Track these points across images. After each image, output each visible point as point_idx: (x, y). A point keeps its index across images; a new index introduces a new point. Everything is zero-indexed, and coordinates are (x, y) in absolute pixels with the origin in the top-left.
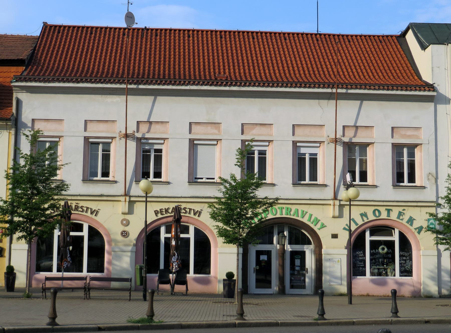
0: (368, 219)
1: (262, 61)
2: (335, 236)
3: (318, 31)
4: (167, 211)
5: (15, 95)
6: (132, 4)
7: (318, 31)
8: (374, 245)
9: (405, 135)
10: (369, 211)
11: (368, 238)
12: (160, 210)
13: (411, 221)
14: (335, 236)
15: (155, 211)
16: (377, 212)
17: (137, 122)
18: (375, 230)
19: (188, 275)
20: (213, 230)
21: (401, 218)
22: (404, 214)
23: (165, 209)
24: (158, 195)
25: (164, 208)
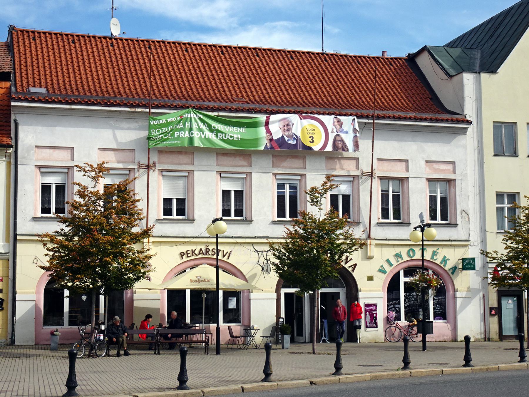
0: (402, 259)
1: (190, 70)
2: (370, 278)
3: (323, 50)
4: (193, 252)
5: (13, 117)
6: (116, 9)
7: (323, 50)
8: (408, 287)
9: (438, 169)
10: (404, 251)
11: (403, 279)
12: (187, 251)
13: (445, 260)
14: (370, 278)
15: (181, 253)
16: (411, 253)
17: (358, 158)
18: (409, 272)
19: (339, 300)
20: (272, 269)
21: (435, 258)
22: (438, 253)
23: (192, 250)
24: (184, 235)
25: (190, 250)
